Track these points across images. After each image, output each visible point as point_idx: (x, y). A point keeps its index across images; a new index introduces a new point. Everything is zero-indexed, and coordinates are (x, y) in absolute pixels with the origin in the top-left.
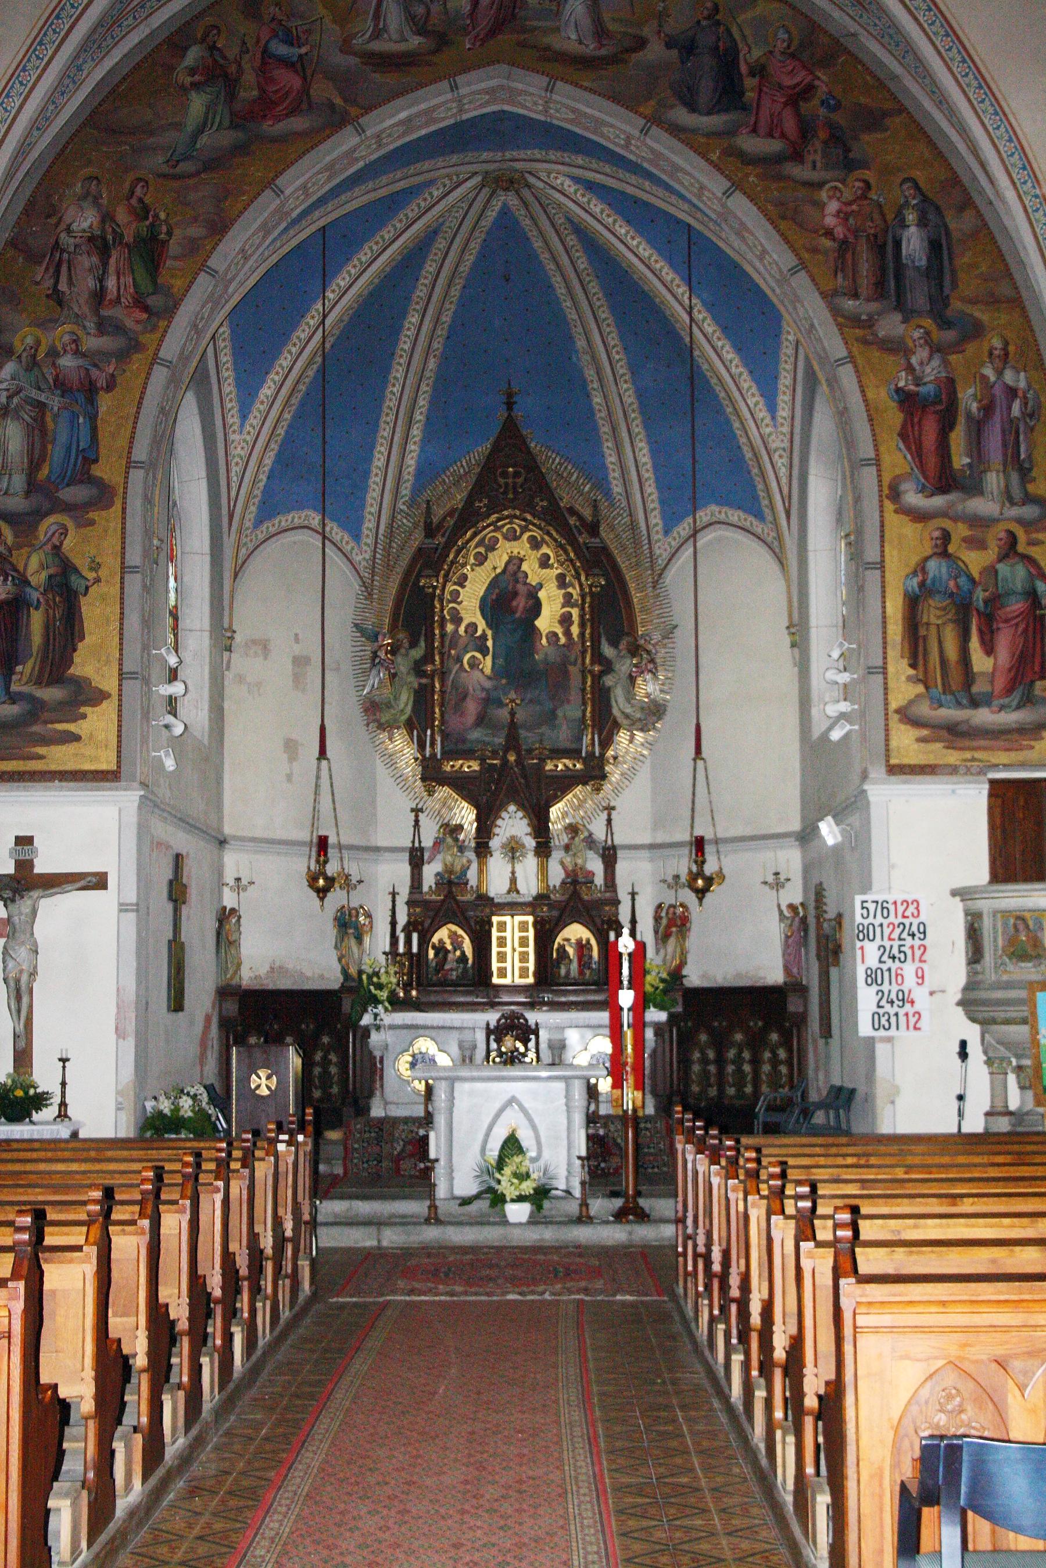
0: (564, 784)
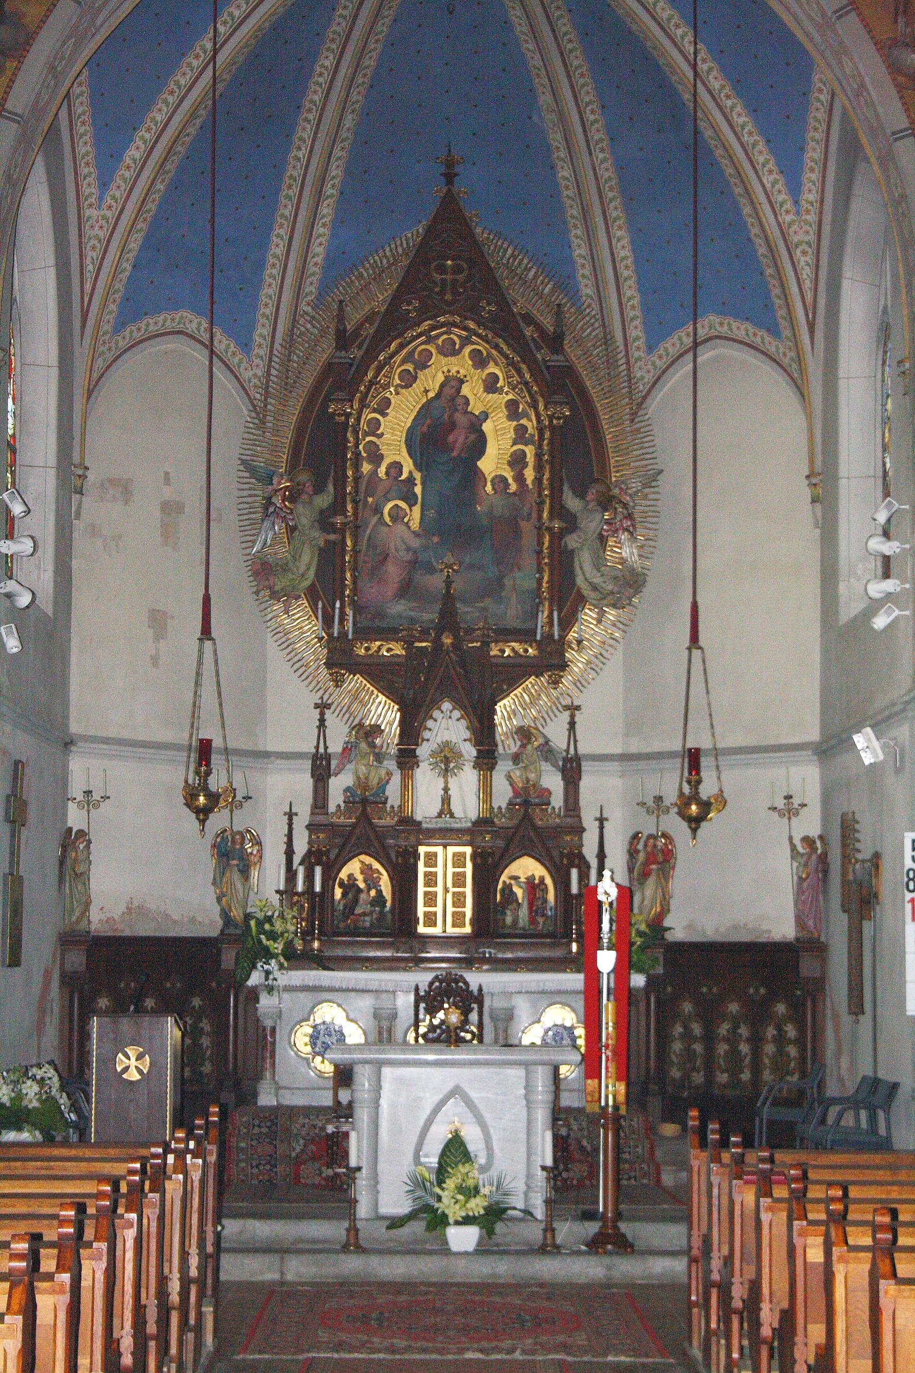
0: (513, 674)
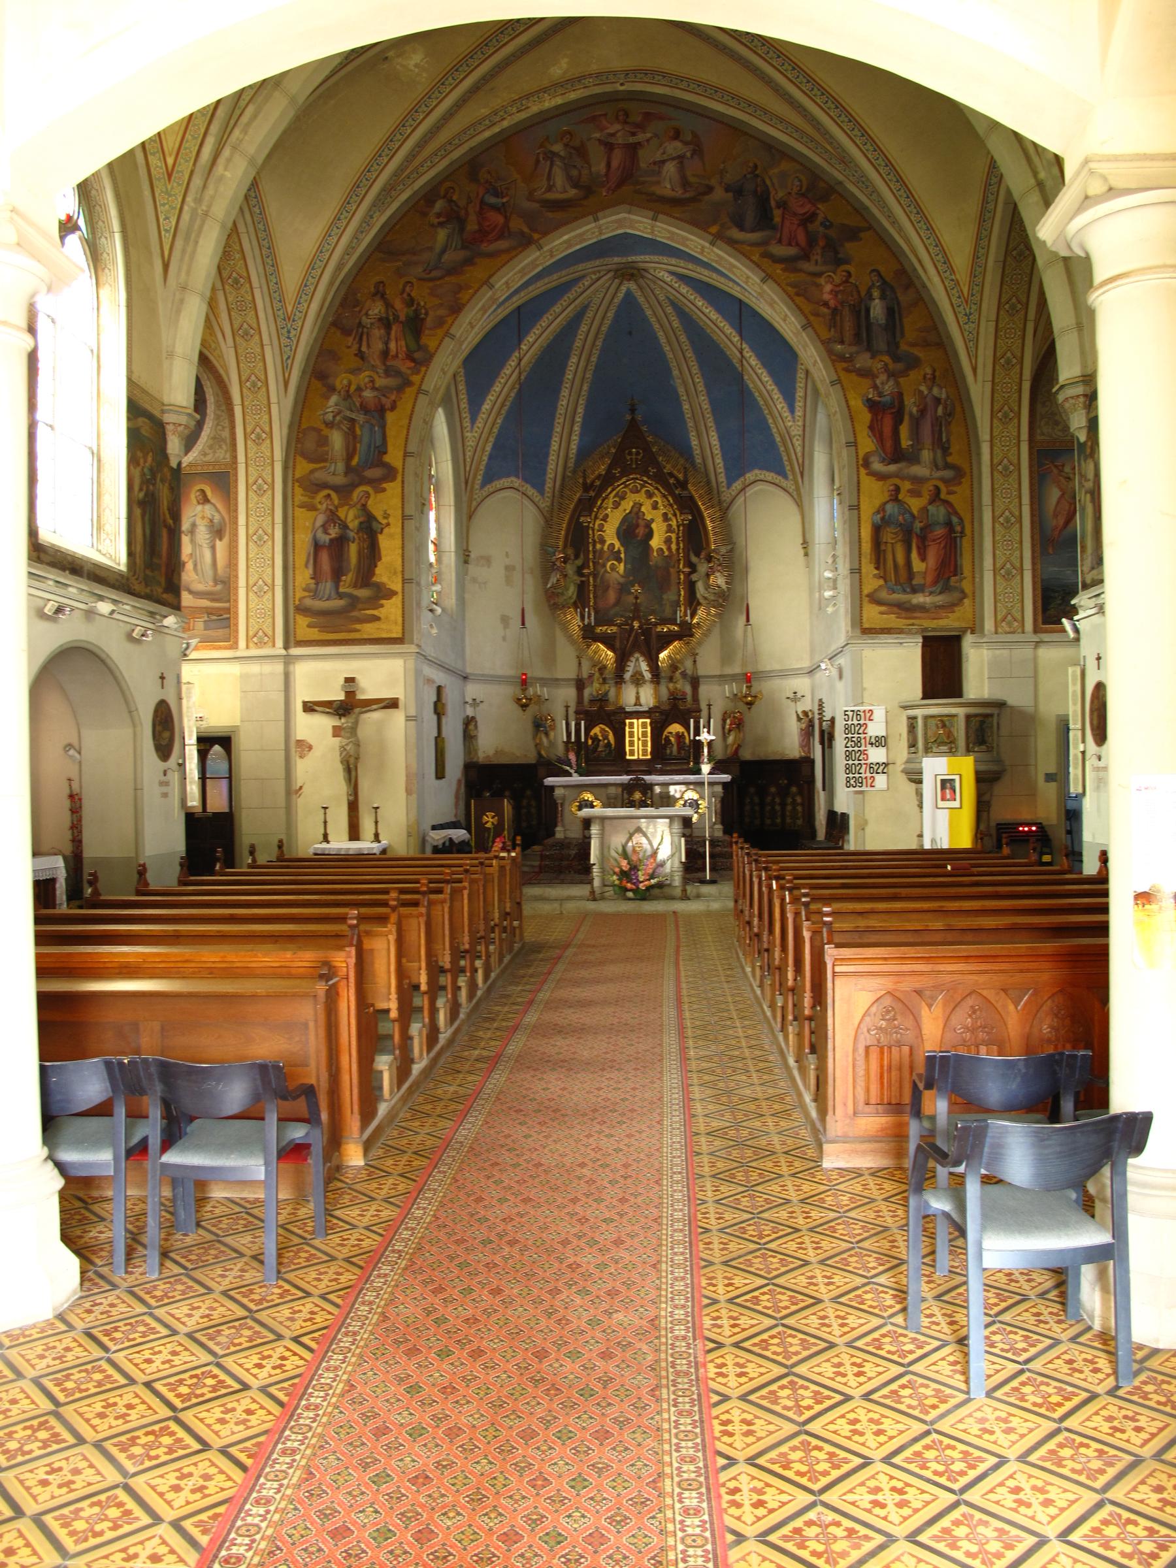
0: (665, 641)
